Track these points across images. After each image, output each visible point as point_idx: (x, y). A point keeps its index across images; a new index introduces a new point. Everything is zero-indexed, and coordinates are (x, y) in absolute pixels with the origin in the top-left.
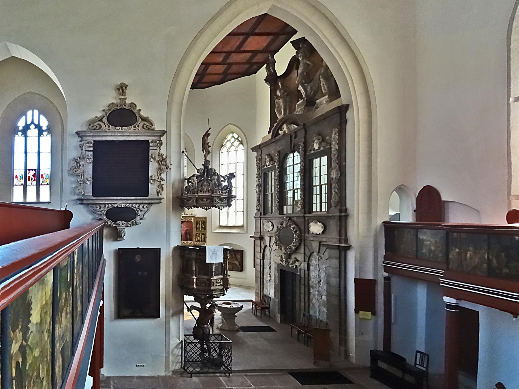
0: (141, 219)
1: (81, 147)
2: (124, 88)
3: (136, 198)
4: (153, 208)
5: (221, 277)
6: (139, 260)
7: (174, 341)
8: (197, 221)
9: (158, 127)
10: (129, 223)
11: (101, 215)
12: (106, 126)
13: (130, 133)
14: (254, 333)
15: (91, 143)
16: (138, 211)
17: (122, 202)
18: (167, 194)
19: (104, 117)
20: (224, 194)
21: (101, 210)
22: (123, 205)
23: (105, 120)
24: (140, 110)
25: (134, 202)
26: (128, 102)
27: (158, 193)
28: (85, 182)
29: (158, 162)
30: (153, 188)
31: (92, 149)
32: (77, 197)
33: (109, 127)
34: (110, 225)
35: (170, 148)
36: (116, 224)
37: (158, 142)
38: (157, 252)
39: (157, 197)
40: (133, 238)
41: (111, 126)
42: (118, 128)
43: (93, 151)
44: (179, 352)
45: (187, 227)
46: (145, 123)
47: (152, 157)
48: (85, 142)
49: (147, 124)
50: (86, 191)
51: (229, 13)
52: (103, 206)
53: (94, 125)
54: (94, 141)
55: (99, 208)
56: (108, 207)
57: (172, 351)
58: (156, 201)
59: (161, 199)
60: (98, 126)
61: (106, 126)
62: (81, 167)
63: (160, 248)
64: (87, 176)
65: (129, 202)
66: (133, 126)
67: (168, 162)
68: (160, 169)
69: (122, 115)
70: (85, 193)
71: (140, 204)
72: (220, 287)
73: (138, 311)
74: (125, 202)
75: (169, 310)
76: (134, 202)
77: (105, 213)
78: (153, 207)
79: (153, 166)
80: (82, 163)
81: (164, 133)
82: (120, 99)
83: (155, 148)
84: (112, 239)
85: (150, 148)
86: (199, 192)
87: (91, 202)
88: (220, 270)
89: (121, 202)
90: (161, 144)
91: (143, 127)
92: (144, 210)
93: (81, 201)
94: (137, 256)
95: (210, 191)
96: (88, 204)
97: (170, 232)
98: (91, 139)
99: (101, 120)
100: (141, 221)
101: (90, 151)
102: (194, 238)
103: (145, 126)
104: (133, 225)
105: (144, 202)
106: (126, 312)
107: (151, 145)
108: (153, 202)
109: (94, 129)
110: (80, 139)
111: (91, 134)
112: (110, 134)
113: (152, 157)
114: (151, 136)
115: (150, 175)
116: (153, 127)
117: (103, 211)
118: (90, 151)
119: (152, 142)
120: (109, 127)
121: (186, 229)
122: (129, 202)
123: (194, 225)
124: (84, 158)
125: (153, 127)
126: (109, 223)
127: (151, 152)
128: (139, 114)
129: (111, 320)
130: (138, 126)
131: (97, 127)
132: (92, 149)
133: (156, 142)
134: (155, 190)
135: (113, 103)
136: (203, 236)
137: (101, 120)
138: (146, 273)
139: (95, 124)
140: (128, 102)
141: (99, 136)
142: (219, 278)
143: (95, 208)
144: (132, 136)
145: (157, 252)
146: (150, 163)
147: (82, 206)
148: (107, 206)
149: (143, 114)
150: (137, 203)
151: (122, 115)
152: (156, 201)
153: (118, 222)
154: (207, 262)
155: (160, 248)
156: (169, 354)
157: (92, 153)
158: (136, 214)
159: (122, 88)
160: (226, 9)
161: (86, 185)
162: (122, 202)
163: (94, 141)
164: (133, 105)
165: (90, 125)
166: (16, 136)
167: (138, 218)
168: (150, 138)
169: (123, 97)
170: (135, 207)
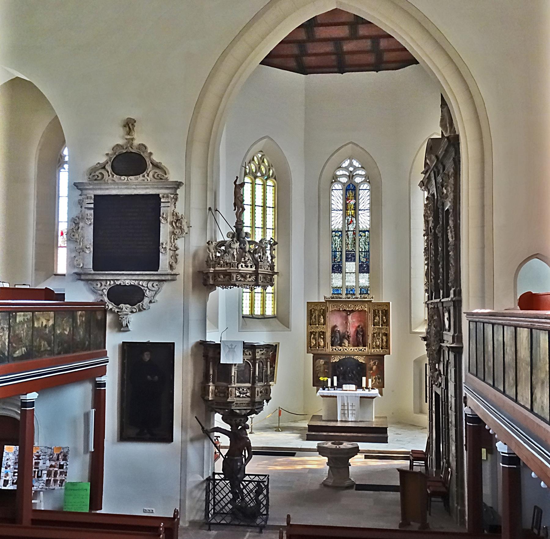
0: (150, 302)
1: (80, 203)
2: (130, 125)
3: (141, 272)
4: (165, 286)
5: (249, 385)
6: (148, 359)
7: (195, 478)
8: (374, 311)
9: (173, 177)
10: (135, 307)
11: (102, 295)
12: (109, 176)
13: (136, 185)
14: (372, 492)
15: (91, 198)
16: (146, 290)
17: (126, 279)
18: (184, 269)
19: (107, 163)
20: (249, 269)
21: (103, 287)
22: (127, 283)
23: (109, 168)
24: (151, 154)
25: (140, 278)
26: (136, 142)
27: (171, 267)
28: (83, 251)
29: (171, 223)
30: (164, 260)
31: (92, 206)
32: (76, 270)
33: (113, 176)
34: (111, 309)
35: (185, 206)
36: (119, 308)
37: (172, 196)
38: (170, 347)
39: (169, 271)
40: (139, 328)
41: (115, 176)
42: (123, 178)
43: (94, 209)
44: (201, 495)
45: (360, 321)
46: (157, 171)
47: (163, 217)
48: (85, 197)
49: (159, 172)
50: (85, 263)
51: (271, 16)
52: (104, 283)
53: (96, 174)
54: (95, 196)
55: (99, 285)
56: (110, 285)
57: (191, 492)
58: (169, 277)
59: (176, 275)
60: (99, 175)
61: (109, 176)
62: (79, 231)
63: (174, 343)
64: (86, 242)
65: (134, 278)
66: (141, 175)
67: (184, 223)
68: (173, 233)
69: (130, 161)
70: (83, 264)
71: (149, 281)
72: (244, 399)
73: (146, 431)
74: (130, 277)
75: (186, 433)
76: (140, 278)
77: (106, 293)
78: (165, 285)
79: (165, 229)
80: (81, 224)
81: (178, 185)
82: (126, 139)
83: (169, 204)
84: (117, 329)
85: (162, 205)
86: (216, 265)
87: (90, 277)
88: (247, 375)
89: (125, 278)
90: (176, 199)
91: (154, 176)
92: (153, 289)
93: (79, 276)
94: (146, 353)
95: (229, 265)
96: (87, 280)
97: (188, 320)
98: (92, 194)
99: (104, 168)
100: (151, 305)
101: (90, 209)
102: (370, 341)
103: (156, 176)
104: (140, 310)
105: (152, 278)
106: (132, 432)
107: (162, 200)
108: (163, 278)
109: (96, 180)
110: (80, 192)
111: (91, 187)
112: (113, 186)
113: (163, 217)
114: (162, 188)
115: (161, 242)
116: (166, 176)
117: (104, 291)
118: (90, 209)
119: (163, 197)
120: (113, 176)
121: (357, 325)
122: (134, 278)
123: (371, 315)
124: (83, 218)
125: (166, 176)
126: (110, 307)
127: (162, 210)
128: (150, 159)
129: (113, 443)
130: (148, 176)
131: (98, 177)
132: (92, 206)
133: (168, 197)
134: (168, 261)
135: (117, 145)
136: (384, 338)
137: (104, 168)
138: (156, 378)
139: (97, 173)
140: (136, 142)
141: (101, 189)
142: (244, 387)
143: (95, 286)
144: (139, 188)
145: (170, 347)
146: (161, 225)
147: (81, 283)
148: (108, 282)
149: (156, 158)
150: (137, 280)
151: (130, 161)
152: (169, 277)
153: (121, 305)
154: (221, 362)
155: (174, 343)
156: (185, 497)
157: (92, 211)
158: (143, 295)
159: (129, 125)
160: (264, 14)
161: (85, 255)
162: (126, 279)
163: (95, 196)
164: (143, 147)
165: (90, 175)
166: (62, 170)
167: (146, 300)
168: (161, 192)
169: (129, 137)
170: (142, 286)
